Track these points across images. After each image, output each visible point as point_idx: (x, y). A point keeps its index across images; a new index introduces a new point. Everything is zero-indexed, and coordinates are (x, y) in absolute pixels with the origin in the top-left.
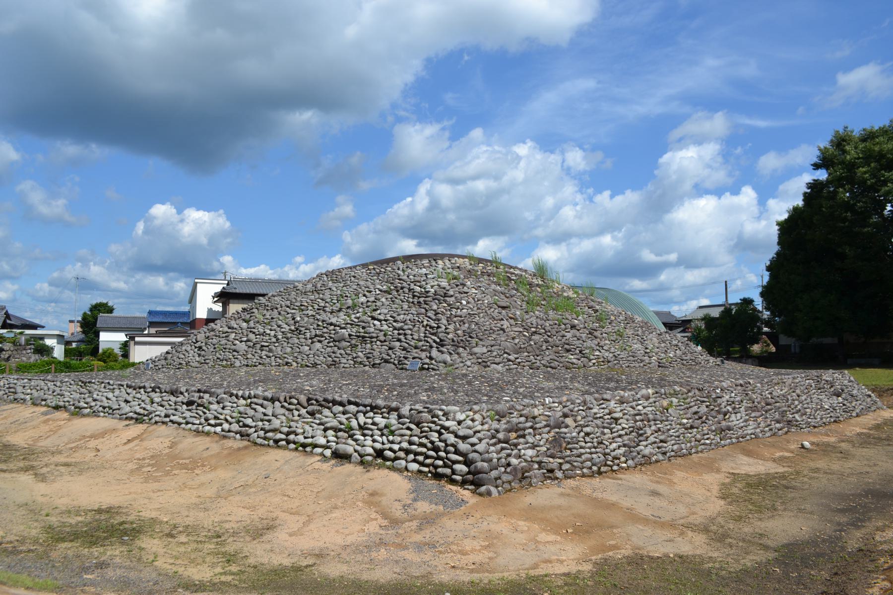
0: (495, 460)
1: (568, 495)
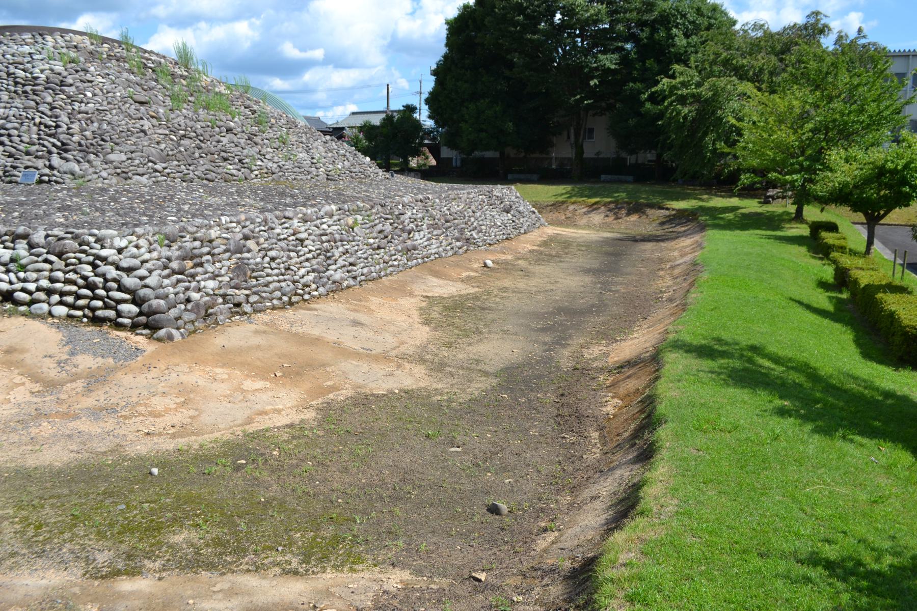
0: (172, 296)
1: (265, 332)
